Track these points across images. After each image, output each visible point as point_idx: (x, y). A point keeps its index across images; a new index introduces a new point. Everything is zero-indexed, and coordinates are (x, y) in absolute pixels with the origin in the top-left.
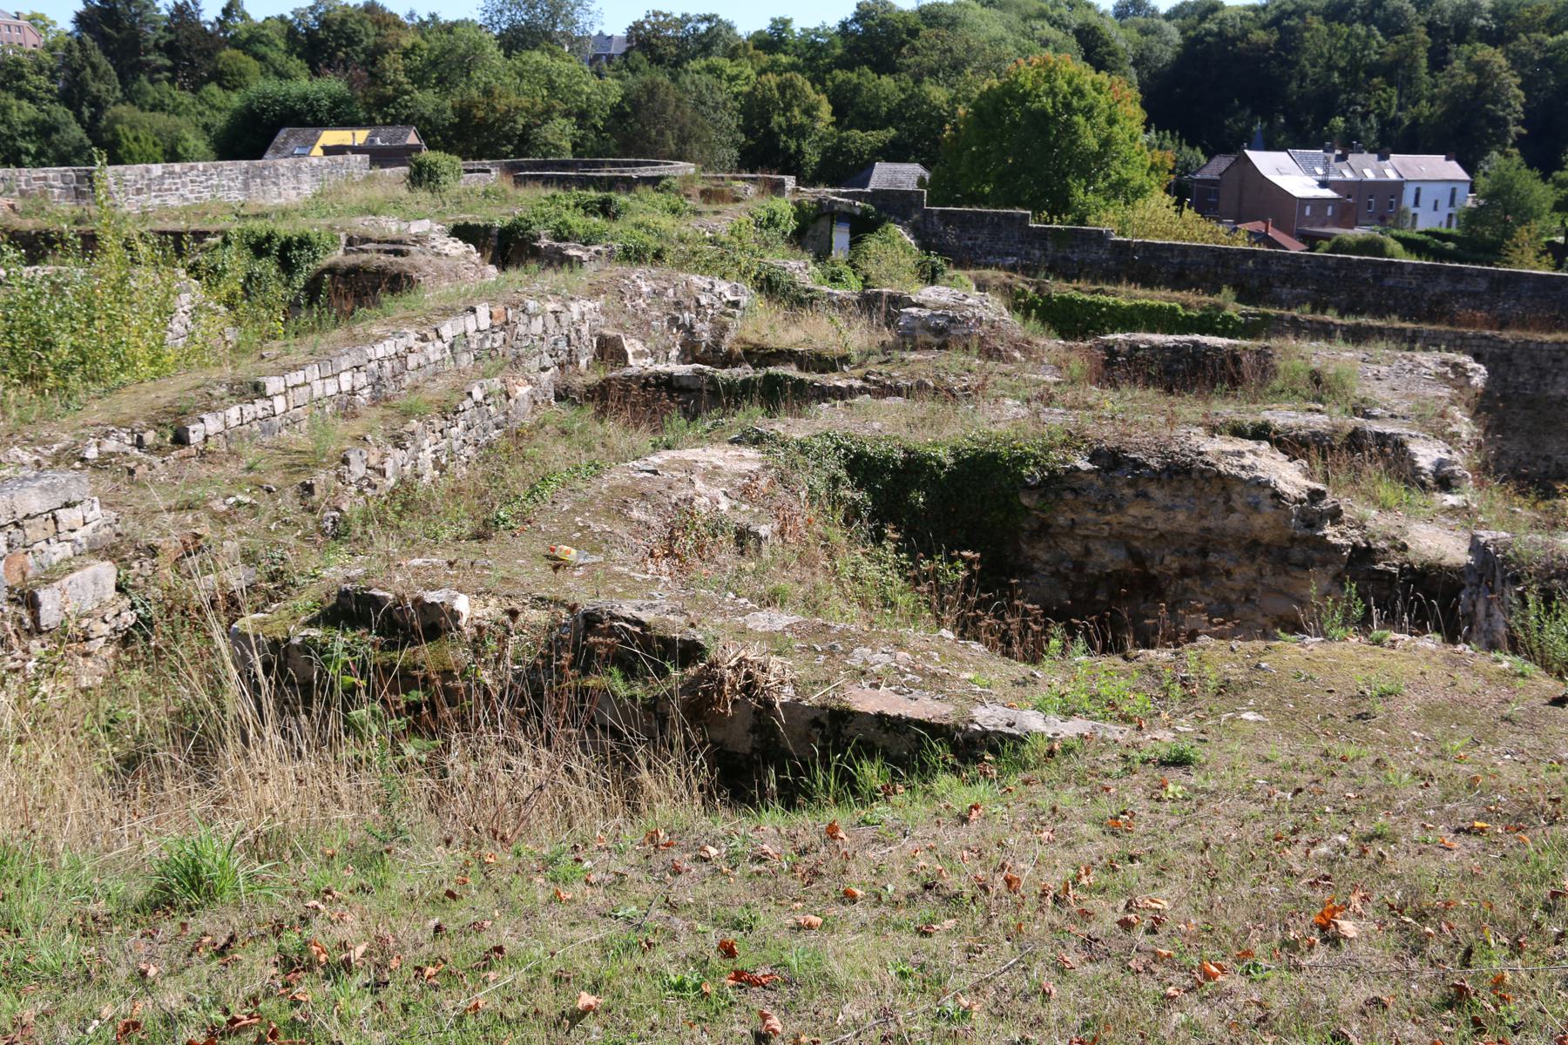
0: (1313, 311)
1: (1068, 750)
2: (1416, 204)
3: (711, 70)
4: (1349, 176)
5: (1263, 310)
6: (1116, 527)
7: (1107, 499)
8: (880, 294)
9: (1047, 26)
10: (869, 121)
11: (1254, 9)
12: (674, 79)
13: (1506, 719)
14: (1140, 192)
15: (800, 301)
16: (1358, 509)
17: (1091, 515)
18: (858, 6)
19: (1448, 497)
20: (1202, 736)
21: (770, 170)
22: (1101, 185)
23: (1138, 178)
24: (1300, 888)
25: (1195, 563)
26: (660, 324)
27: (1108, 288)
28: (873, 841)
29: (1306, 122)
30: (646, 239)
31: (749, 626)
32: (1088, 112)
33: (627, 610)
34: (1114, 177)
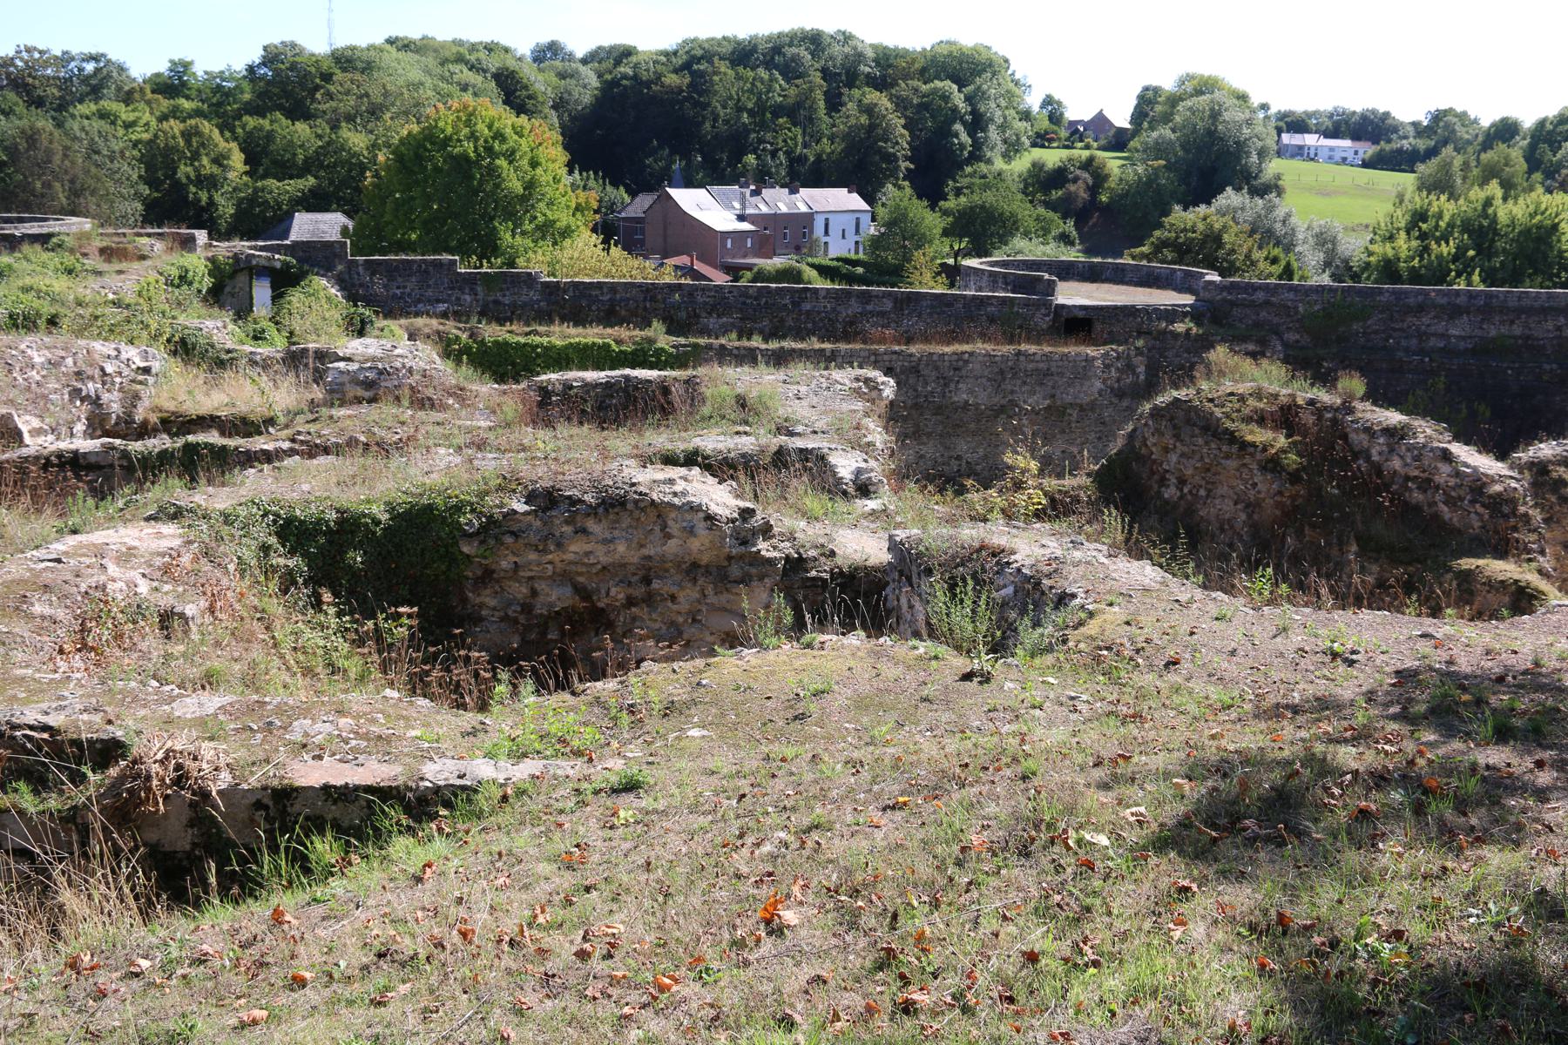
0: (740, 338)
1: (521, 793)
2: (827, 233)
3: (103, 115)
4: (764, 209)
5: (693, 340)
6: (559, 565)
7: (546, 539)
8: (305, 350)
9: (465, 70)
10: (285, 170)
11: (666, 54)
12: (59, 125)
13: (925, 700)
14: (566, 233)
15: (220, 362)
16: (787, 522)
17: (533, 556)
18: (265, 49)
19: (868, 502)
20: (651, 759)
21: (178, 225)
22: (528, 227)
23: (564, 218)
24: (747, 888)
25: (638, 592)
26: (60, 397)
27: (541, 329)
28: (324, 919)
29: (721, 160)
30: (36, 304)
31: (177, 714)
32: (511, 156)
33: (31, 716)
34: (541, 219)
